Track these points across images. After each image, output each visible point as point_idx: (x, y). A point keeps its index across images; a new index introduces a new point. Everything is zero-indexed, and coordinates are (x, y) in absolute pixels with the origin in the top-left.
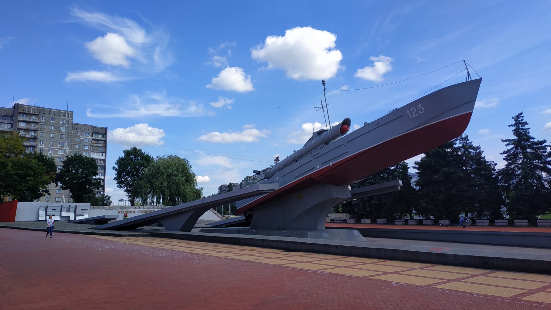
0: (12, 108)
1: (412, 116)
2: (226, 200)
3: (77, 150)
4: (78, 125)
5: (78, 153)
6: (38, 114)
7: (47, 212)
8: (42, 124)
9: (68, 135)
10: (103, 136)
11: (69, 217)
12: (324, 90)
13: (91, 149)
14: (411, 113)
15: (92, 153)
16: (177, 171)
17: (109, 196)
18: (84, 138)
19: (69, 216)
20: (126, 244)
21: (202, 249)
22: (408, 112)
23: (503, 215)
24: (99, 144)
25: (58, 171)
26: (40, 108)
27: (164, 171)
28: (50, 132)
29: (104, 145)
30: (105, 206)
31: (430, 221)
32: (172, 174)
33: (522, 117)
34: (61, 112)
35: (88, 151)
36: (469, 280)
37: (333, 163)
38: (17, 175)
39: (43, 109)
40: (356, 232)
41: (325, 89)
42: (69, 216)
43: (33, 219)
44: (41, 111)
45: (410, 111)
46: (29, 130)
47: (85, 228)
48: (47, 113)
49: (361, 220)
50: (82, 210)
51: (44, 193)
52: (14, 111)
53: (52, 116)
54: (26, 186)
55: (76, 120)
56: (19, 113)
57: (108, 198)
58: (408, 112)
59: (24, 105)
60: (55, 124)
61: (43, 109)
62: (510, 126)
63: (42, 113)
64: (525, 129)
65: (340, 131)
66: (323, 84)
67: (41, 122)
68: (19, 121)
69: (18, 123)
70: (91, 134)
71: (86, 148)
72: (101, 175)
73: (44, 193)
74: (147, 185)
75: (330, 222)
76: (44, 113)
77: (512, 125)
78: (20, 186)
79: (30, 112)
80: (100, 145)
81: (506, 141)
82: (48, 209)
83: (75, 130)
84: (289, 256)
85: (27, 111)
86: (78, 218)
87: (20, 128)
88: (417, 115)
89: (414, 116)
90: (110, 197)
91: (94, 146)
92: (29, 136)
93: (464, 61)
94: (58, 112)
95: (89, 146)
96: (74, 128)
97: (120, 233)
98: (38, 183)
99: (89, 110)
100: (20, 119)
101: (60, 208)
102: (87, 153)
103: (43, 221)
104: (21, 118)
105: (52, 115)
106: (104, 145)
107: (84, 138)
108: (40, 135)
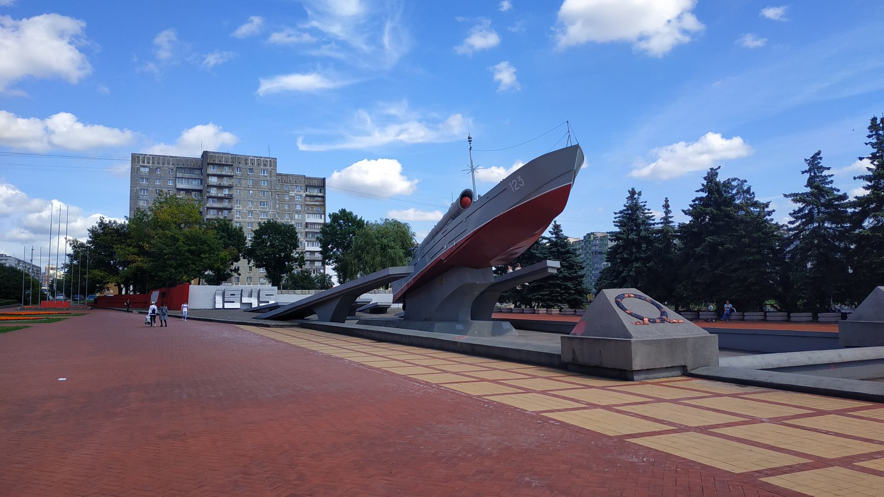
0: (200, 157)
1: (514, 190)
5: (272, 219)
6: (232, 164)
8: (237, 177)
9: (271, 192)
10: (320, 190)
12: (470, 149)
13: (305, 210)
14: (513, 185)
15: (306, 215)
17: (330, 275)
19: (251, 303)
21: (417, 365)
23: (733, 305)
24: (315, 201)
25: (249, 244)
26: (234, 156)
28: (248, 189)
29: (322, 203)
30: (296, 291)
31: (689, 313)
32: (388, 246)
33: (821, 158)
35: (302, 213)
36: (699, 395)
38: (189, 251)
39: (237, 157)
40: (507, 325)
41: (471, 147)
42: (251, 303)
43: (209, 306)
44: (235, 159)
45: (511, 183)
46: (222, 186)
48: (243, 162)
49: (819, 315)
50: (266, 295)
51: (233, 272)
52: (202, 161)
54: (200, 265)
55: (281, 170)
56: (209, 164)
58: (510, 184)
59: (214, 153)
61: (237, 157)
62: (803, 173)
64: (823, 177)
65: (460, 206)
66: (469, 141)
67: (236, 175)
68: (209, 175)
69: (208, 178)
70: (303, 188)
71: (299, 208)
73: (233, 273)
75: (574, 314)
77: (806, 171)
78: (193, 266)
79: (221, 163)
80: (317, 203)
81: (790, 195)
82: (225, 294)
86: (227, 306)
87: (210, 184)
89: (516, 189)
90: (331, 277)
91: (308, 205)
92: (223, 195)
93: (568, 122)
94: (257, 159)
95: (301, 205)
96: (280, 180)
97: (264, 323)
98: (214, 261)
99: (300, 140)
100: (210, 173)
102: (300, 216)
103: (221, 309)
104: (211, 170)
106: (322, 203)
108: (235, 193)
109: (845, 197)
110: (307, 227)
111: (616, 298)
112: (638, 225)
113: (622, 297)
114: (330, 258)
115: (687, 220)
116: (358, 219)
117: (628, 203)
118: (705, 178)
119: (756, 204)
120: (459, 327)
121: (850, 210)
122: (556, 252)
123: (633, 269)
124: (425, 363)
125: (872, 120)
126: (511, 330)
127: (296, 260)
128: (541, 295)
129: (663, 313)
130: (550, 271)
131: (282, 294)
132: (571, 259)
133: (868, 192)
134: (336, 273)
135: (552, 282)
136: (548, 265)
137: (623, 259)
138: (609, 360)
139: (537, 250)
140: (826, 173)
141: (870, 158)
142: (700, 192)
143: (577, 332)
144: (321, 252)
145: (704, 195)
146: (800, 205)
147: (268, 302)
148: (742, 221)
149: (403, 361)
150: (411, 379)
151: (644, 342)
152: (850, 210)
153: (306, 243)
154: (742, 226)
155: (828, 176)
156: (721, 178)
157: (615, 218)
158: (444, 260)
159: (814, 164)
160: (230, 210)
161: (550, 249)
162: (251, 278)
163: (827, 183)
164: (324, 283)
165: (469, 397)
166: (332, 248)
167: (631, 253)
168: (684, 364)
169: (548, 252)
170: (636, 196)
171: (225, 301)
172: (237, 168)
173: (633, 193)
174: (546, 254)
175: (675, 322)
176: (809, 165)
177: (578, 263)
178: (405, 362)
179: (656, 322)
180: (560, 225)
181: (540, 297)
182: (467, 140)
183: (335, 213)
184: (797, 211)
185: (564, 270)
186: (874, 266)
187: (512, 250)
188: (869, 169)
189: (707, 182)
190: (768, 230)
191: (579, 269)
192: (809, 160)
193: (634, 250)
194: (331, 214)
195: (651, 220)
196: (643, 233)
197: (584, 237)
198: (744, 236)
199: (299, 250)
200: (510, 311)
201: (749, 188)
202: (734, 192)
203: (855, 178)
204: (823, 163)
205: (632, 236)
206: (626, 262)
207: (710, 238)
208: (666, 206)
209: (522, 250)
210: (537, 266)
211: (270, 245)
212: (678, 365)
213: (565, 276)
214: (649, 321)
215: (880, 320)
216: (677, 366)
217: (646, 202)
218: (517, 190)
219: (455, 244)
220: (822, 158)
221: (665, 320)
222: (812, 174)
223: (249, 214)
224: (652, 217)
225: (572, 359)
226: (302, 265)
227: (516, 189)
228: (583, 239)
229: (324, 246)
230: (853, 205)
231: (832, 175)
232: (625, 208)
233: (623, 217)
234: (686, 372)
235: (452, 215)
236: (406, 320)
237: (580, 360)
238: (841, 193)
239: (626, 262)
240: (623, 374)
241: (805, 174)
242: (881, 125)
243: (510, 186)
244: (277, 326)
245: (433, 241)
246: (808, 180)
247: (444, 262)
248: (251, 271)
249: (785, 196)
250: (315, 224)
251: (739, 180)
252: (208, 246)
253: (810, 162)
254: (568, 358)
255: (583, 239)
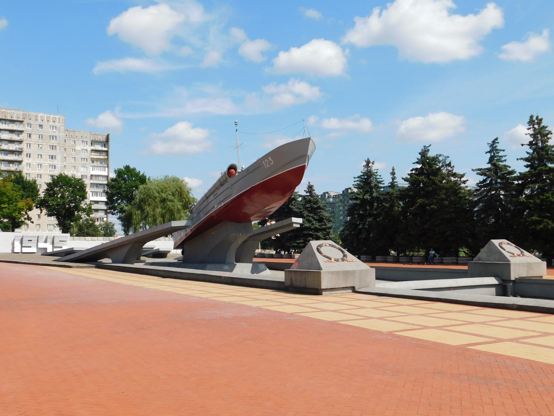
1: (267, 167)
2: (139, 238)
3: (72, 164)
4: (73, 132)
6: (23, 120)
7: (23, 243)
9: (60, 146)
11: (46, 249)
16: (173, 195)
18: (81, 148)
20: (70, 274)
21: (193, 290)
22: (264, 163)
25: (42, 195)
27: (157, 195)
29: (106, 157)
30: (86, 237)
34: (50, 117)
37: (224, 203)
40: (263, 266)
41: (237, 130)
45: (265, 162)
47: (50, 260)
50: (60, 241)
51: (27, 220)
53: (39, 123)
57: (112, 226)
58: (264, 163)
60: (44, 133)
63: (27, 119)
64: (499, 157)
66: (235, 125)
67: (27, 131)
70: (89, 143)
72: (104, 196)
74: (269, 159)
76: (30, 119)
77: (488, 152)
81: (476, 170)
82: (23, 240)
83: (69, 138)
84: (318, 302)
85: (10, 117)
86: (25, 250)
88: (269, 166)
89: (267, 167)
90: (113, 225)
94: (46, 116)
101: (37, 239)
103: (19, 253)
105: (39, 121)
107: (81, 148)
108: (24, 146)
109: (513, 172)
110: (91, 179)
111: (317, 246)
112: (371, 188)
113: (320, 246)
114: (114, 208)
115: (406, 185)
116: (141, 174)
117: (364, 170)
118: (420, 154)
119: (455, 175)
120: (226, 267)
121: (516, 182)
122: (310, 208)
123: (367, 223)
124: (200, 289)
125: (530, 117)
126: (265, 270)
127: (84, 210)
128: (297, 243)
129: (345, 256)
130: (295, 225)
131: (74, 240)
132: (322, 213)
133: (528, 169)
134: (120, 222)
135: (306, 232)
136: (293, 221)
137: (359, 215)
138: (310, 283)
139: (294, 206)
140: (501, 154)
141: (529, 145)
142: (416, 164)
143: (292, 269)
144: (106, 203)
145: (419, 166)
146: (482, 178)
147: (61, 247)
148: (444, 188)
149: (184, 288)
150: (190, 296)
151: (329, 272)
152: (516, 182)
153: (91, 193)
154: (444, 191)
155: (503, 156)
156: (431, 154)
157: (355, 181)
158: (215, 216)
159: (493, 148)
160: (20, 162)
161: (305, 205)
162: (40, 225)
163: (502, 161)
164: (109, 231)
165: (224, 302)
166: (117, 200)
167: (366, 210)
168: (353, 286)
169: (303, 207)
170: (370, 165)
171: (23, 246)
172: (28, 124)
173: (368, 162)
174: (301, 209)
175: (351, 261)
176: (490, 148)
177: (327, 217)
178: (185, 289)
179: (339, 261)
180: (313, 185)
181: (296, 245)
182: (234, 123)
183: (121, 169)
184: (482, 182)
185: (316, 223)
186: (527, 224)
187: (267, 209)
188: (528, 153)
189: (421, 157)
190: (462, 195)
191: (328, 222)
192: (490, 144)
193: (368, 208)
194: (117, 169)
195: (381, 184)
196: (375, 194)
197: (343, 191)
198: (445, 199)
199: (87, 201)
200: (271, 256)
201: (450, 163)
202: (440, 165)
203: (517, 159)
204: (499, 147)
205: (367, 197)
206: (362, 218)
207: (421, 200)
208: (393, 173)
209: (274, 210)
210: (285, 222)
211: (61, 197)
212: (350, 286)
213: (316, 228)
214: (335, 260)
215: (490, 261)
216: (349, 287)
217: (378, 170)
218: (268, 167)
219: (223, 205)
220: (499, 142)
221: (344, 260)
222: (492, 154)
223: (38, 166)
224: (382, 181)
225: (291, 284)
226: (90, 214)
227: (267, 167)
228: (342, 193)
229: (110, 197)
230: (517, 178)
231: (506, 156)
232: (362, 174)
233: (360, 181)
234: (354, 290)
235: (221, 183)
236: (184, 262)
237: (295, 284)
238: (510, 169)
239: (362, 218)
240: (317, 291)
241: (488, 154)
242: (536, 121)
243: (264, 164)
244: (78, 267)
245: (207, 201)
246: (489, 158)
247: (215, 218)
248: (40, 218)
249: (473, 170)
250: (99, 176)
251: (444, 156)
252: (7, 197)
253: (491, 145)
254: (288, 284)
255: (342, 193)
